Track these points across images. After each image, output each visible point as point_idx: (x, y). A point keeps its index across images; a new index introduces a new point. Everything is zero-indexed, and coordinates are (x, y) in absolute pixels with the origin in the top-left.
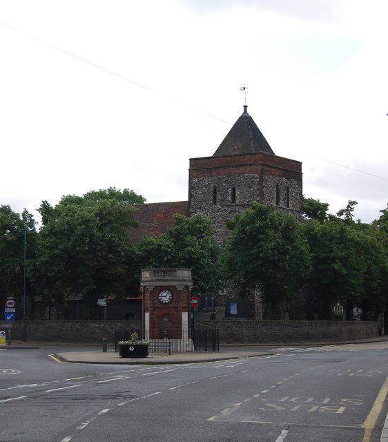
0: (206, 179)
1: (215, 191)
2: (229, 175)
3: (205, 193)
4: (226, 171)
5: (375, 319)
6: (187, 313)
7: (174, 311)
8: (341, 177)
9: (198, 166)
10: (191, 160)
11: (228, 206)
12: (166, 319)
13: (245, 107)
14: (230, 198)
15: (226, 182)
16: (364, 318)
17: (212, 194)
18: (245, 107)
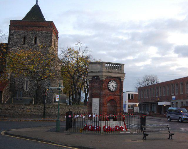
0: (19, 31)
1: (25, 38)
9: (14, 25)
13: (37, 1)
15: (31, 34)
17: (23, 39)
18: (37, 1)
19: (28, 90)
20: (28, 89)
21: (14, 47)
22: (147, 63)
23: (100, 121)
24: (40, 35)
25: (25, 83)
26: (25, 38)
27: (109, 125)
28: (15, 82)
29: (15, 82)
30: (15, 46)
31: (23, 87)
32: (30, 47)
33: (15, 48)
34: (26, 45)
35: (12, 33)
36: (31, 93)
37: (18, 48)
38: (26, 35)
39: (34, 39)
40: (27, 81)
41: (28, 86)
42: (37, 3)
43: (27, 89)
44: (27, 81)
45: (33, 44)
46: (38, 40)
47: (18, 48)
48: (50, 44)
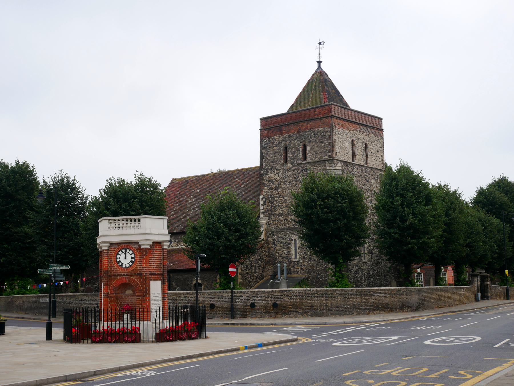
0: (276, 137)
1: (286, 149)
2: (299, 131)
3: (276, 152)
4: (297, 128)
5: (470, 283)
6: (159, 283)
7: (137, 279)
8: (445, 142)
9: (271, 126)
10: (261, 119)
11: (299, 164)
12: (129, 292)
13: (319, 62)
14: (301, 155)
15: (296, 139)
16: (458, 281)
17: (282, 153)
18: (319, 62)
19: (298, 260)
20: (298, 257)
21: (270, 172)
22: (462, 174)
23: (165, 321)
24: (311, 138)
25: (293, 245)
26: (286, 149)
27: (150, 325)
28: (275, 245)
29: (275, 245)
30: (271, 169)
31: (289, 253)
32: (296, 167)
33: (272, 175)
34: (289, 165)
35: (265, 144)
36: (304, 265)
37: (276, 172)
38: (287, 143)
39: (301, 149)
40: (295, 240)
41: (298, 250)
42: (319, 67)
43: (296, 258)
44: (295, 240)
45: (300, 159)
46: (308, 149)
47: (276, 172)
48: (330, 154)
